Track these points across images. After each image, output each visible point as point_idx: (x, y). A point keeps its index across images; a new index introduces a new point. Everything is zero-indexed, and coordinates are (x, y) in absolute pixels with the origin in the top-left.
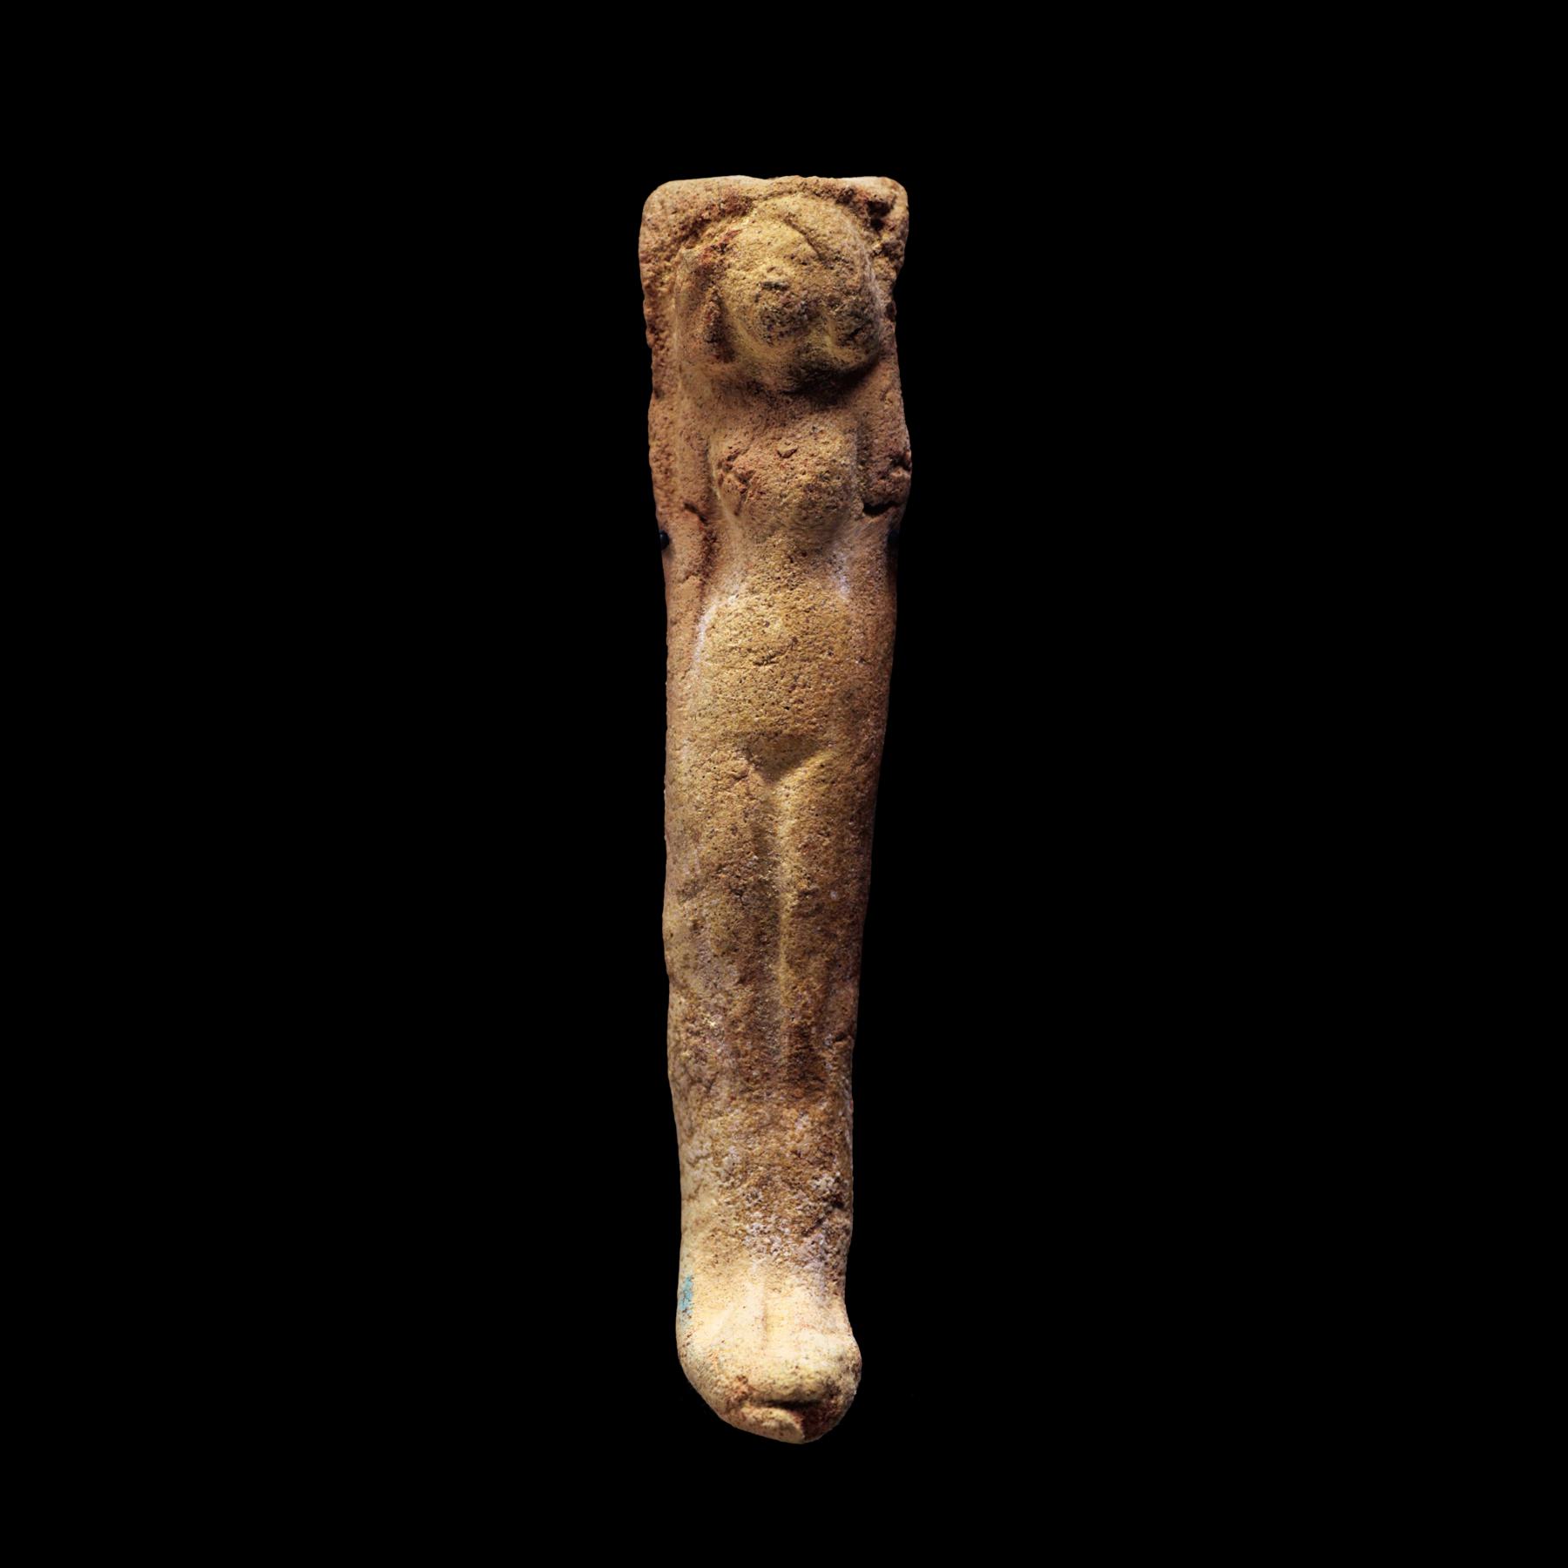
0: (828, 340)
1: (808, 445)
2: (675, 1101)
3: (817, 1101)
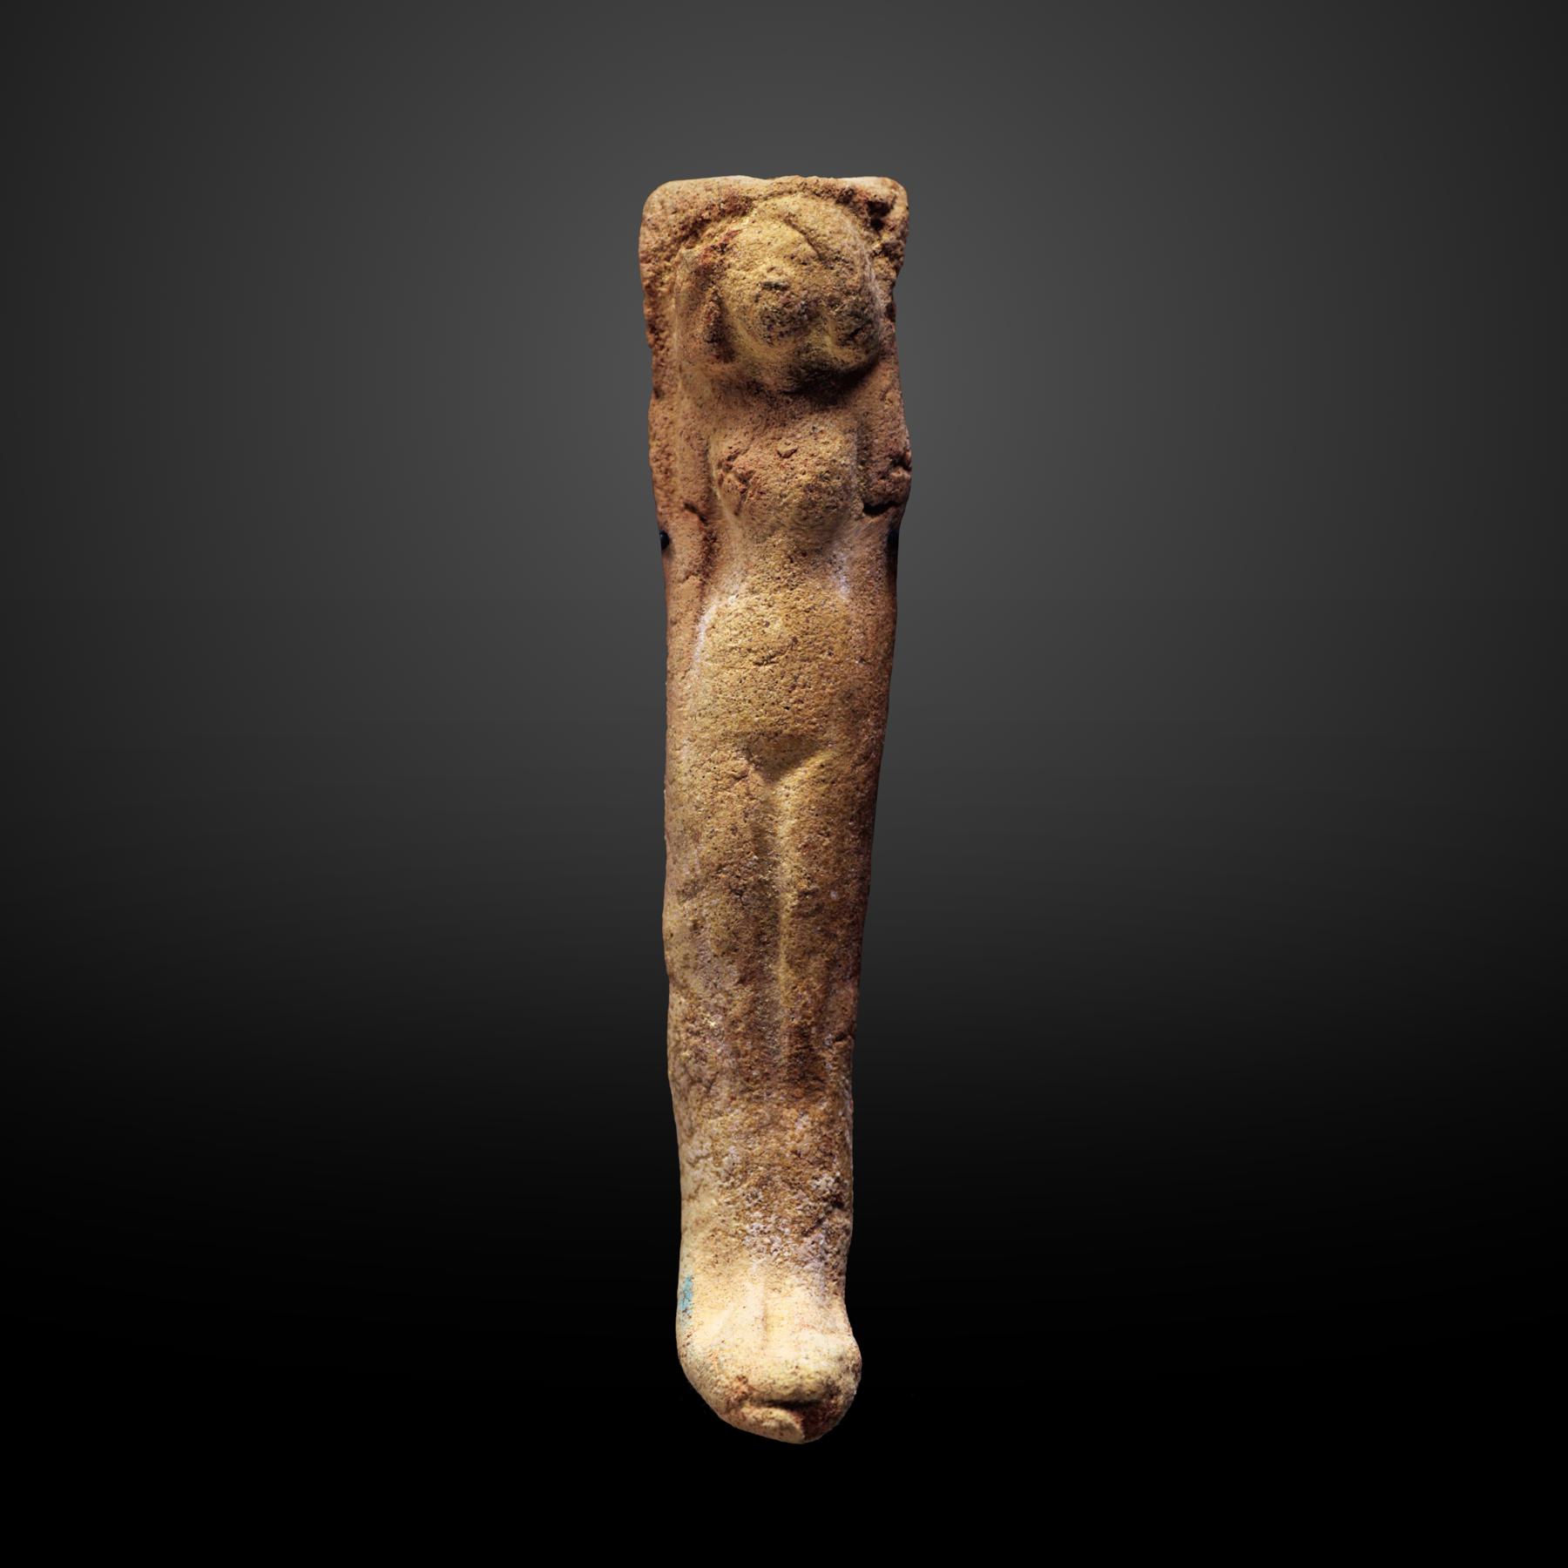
0: (828, 340)
1: (808, 445)
2: (675, 1101)
3: (817, 1101)
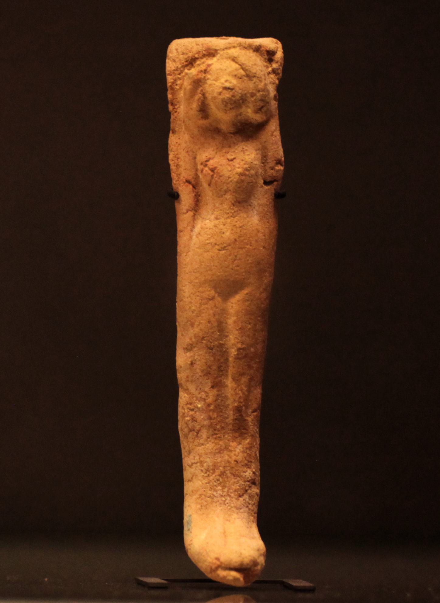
0: (249, 110)
1: (240, 156)
2: (182, 438)
3: (245, 439)
